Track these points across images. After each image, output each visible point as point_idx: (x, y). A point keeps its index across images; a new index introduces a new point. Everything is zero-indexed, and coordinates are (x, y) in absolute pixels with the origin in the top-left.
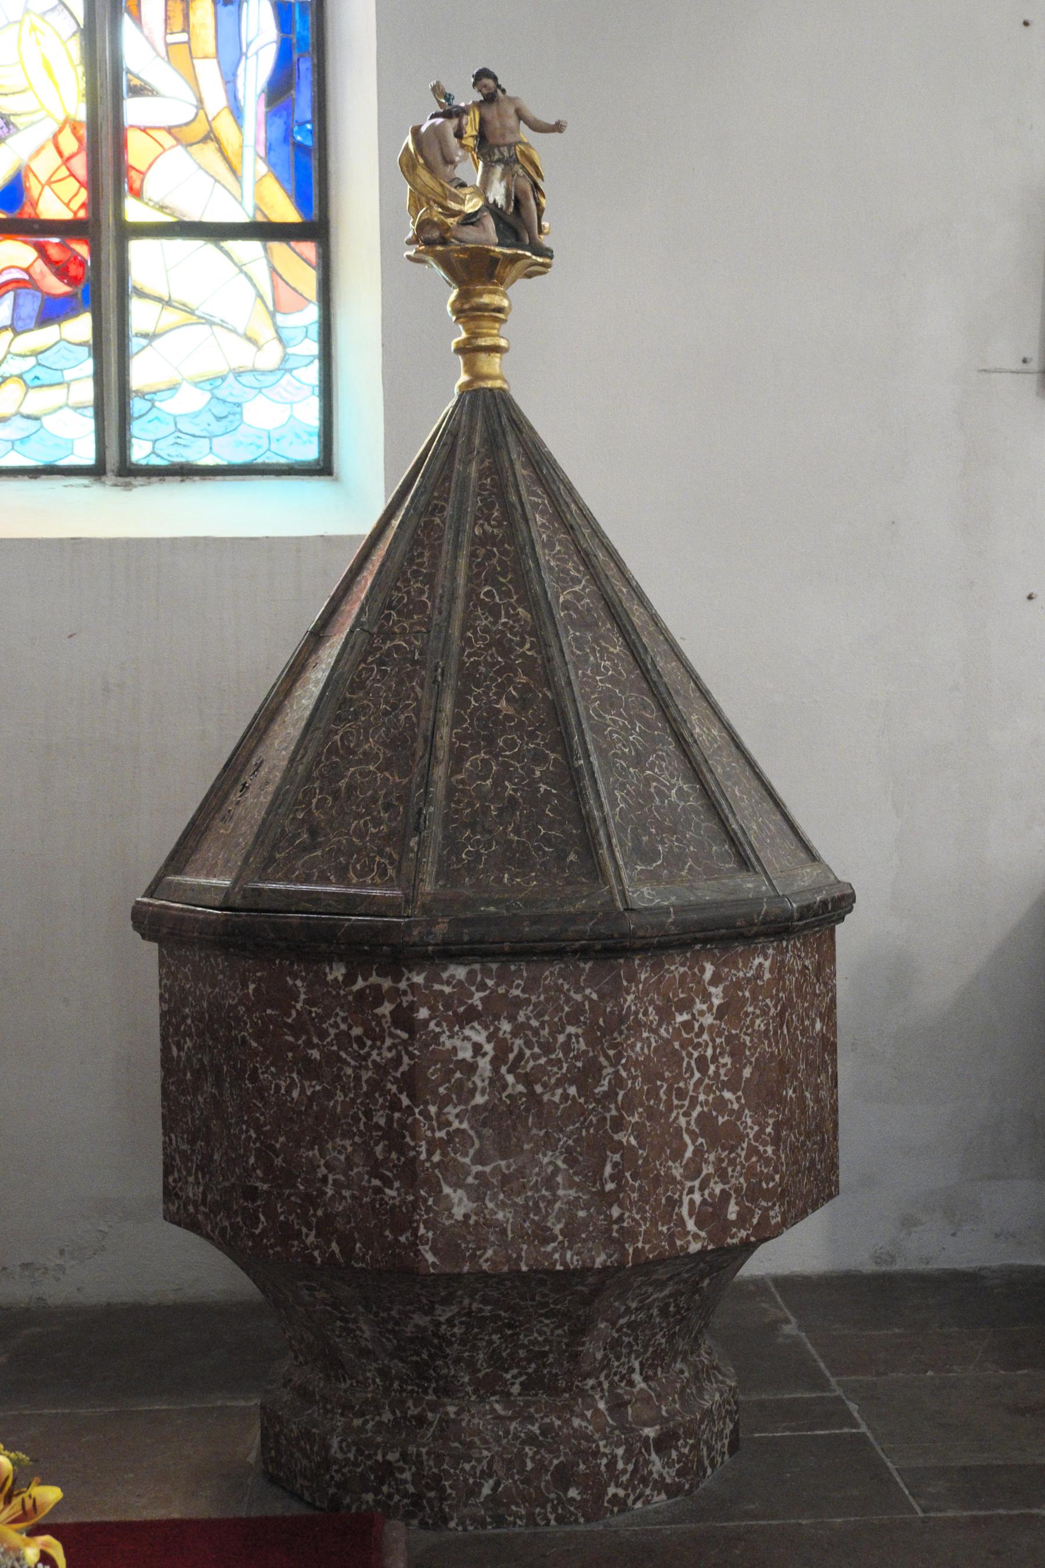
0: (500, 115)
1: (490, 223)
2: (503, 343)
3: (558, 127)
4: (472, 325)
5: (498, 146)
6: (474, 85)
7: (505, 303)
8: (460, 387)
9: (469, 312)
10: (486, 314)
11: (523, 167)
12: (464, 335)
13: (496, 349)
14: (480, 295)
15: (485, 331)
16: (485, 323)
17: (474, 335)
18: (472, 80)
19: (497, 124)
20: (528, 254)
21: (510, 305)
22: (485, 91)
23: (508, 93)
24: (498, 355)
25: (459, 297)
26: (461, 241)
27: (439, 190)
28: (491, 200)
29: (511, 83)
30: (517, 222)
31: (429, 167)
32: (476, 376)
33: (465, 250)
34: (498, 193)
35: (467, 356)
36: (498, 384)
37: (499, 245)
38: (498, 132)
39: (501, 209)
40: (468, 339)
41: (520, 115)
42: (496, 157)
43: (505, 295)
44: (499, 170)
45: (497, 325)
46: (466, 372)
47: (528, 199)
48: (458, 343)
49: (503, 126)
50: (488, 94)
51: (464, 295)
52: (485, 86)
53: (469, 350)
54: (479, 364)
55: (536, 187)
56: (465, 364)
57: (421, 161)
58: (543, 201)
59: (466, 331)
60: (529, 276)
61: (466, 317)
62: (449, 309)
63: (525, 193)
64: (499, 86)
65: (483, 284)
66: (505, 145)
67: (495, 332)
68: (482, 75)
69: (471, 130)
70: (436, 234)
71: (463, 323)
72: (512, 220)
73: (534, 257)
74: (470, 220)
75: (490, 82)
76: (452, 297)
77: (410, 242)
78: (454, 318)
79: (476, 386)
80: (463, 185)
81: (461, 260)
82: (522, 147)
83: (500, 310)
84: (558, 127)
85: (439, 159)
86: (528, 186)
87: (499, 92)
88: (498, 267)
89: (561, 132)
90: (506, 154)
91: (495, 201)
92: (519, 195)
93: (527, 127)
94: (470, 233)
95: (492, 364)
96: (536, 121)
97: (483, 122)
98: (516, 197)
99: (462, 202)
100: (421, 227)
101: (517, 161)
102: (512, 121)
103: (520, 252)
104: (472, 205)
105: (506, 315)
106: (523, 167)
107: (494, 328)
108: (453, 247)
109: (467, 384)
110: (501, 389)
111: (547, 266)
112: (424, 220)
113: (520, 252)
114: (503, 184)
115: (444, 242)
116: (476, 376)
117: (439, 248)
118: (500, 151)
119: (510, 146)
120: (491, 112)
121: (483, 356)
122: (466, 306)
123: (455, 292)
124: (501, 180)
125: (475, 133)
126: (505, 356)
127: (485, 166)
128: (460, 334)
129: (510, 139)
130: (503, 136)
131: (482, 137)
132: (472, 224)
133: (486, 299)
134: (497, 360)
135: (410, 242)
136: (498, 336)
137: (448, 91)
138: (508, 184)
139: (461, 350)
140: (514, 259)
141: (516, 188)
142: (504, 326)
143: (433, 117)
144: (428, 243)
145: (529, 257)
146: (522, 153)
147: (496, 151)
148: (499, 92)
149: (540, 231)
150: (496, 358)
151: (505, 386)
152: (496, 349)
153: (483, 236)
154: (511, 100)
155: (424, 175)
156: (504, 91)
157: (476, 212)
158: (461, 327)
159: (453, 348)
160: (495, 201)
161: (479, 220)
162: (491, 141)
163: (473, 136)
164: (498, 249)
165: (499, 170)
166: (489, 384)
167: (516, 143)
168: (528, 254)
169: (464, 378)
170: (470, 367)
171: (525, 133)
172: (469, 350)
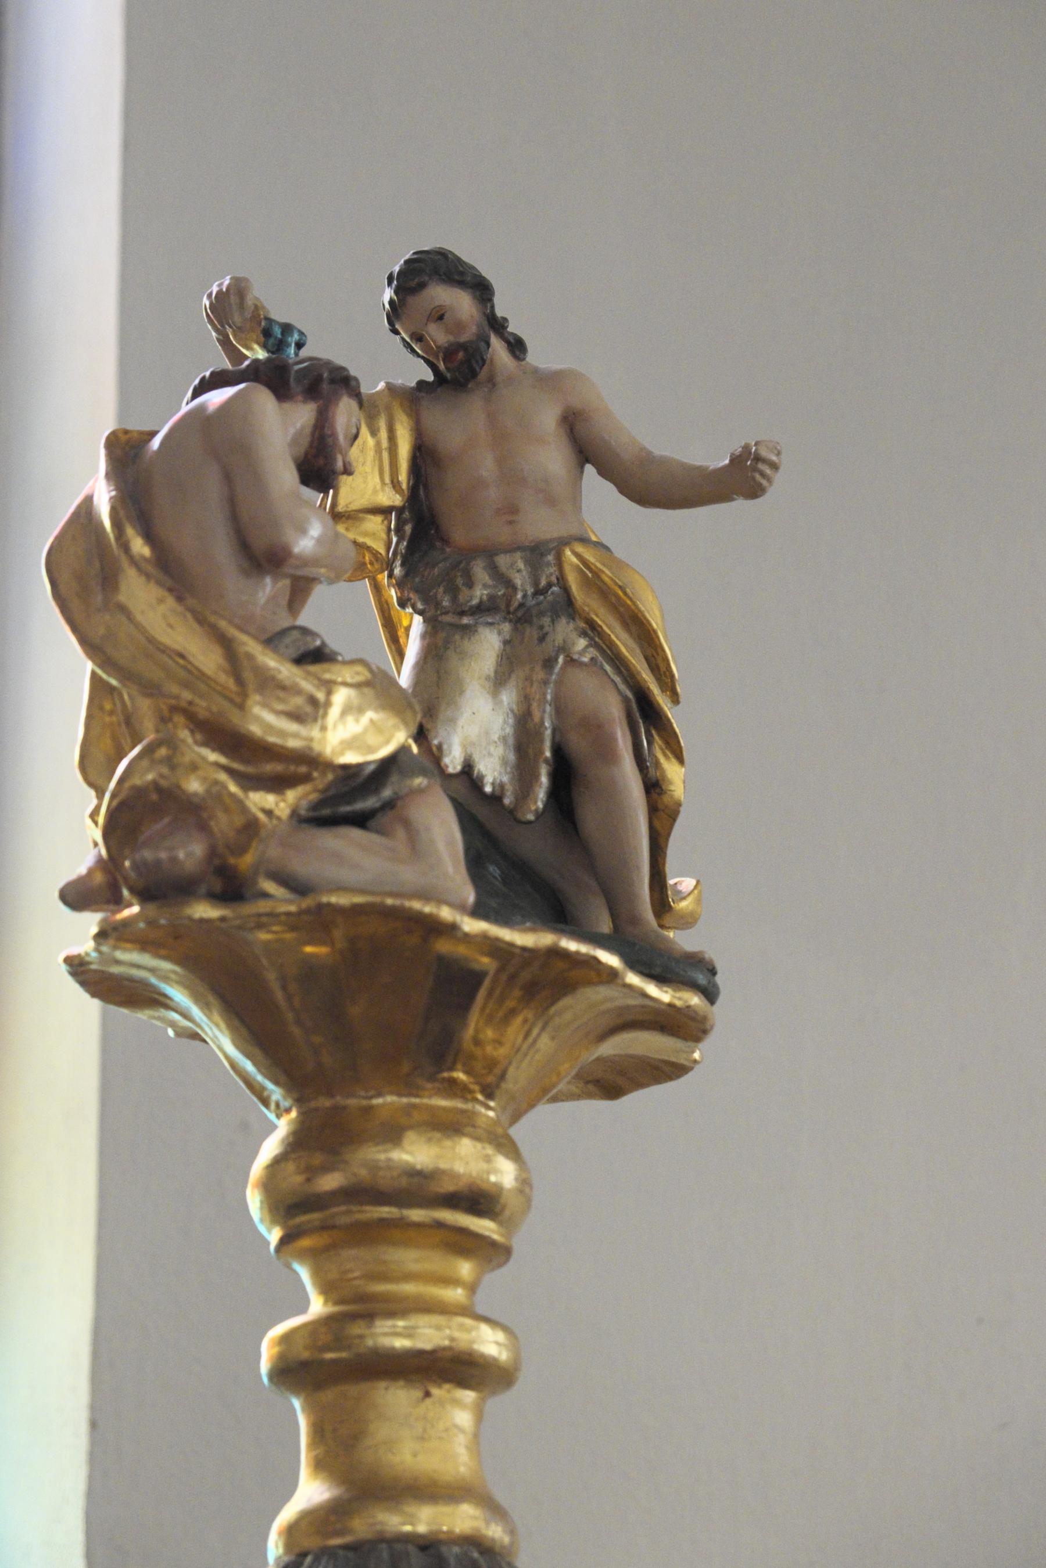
0: (500, 439)
1: (441, 828)
2: (490, 1343)
3: (744, 476)
4: (354, 1260)
5: (490, 553)
6: (395, 313)
7: (504, 1173)
8: (291, 1531)
9: (334, 1209)
10: (417, 1215)
11: (592, 631)
12: (317, 1306)
13: (456, 1368)
14: (393, 1135)
15: (409, 1288)
16: (409, 1258)
17: (357, 1306)
18: (388, 294)
19: (486, 466)
20: (610, 959)
21: (524, 1183)
22: (438, 336)
23: (535, 357)
24: (469, 1396)
25: (298, 1143)
26: (299, 887)
27: (208, 659)
28: (453, 762)
29: (557, 320)
30: (561, 841)
31: (171, 571)
32: (364, 1484)
33: (319, 921)
34: (480, 730)
35: (328, 1395)
36: (463, 1519)
37: (478, 912)
38: (493, 494)
39: (495, 799)
40: (327, 1321)
41: (586, 446)
42: (479, 594)
43: (510, 1148)
44: (488, 644)
45: (465, 1268)
46: (320, 1466)
47: (607, 753)
48: (286, 1339)
49: (512, 476)
50: (449, 353)
51: (316, 1141)
52: (440, 316)
53: (333, 1371)
54: (380, 1431)
55: (646, 713)
56: (318, 1432)
57: (140, 547)
58: (674, 773)
59: (327, 1289)
60: (610, 1083)
61: (325, 1227)
62: (254, 1201)
63: (595, 729)
64: (497, 325)
65: (409, 1087)
66: (512, 549)
67: (456, 1294)
68: (427, 271)
69: (371, 480)
70: (189, 853)
71: (315, 1257)
72: (538, 848)
73: (633, 979)
74: (355, 799)
75: (461, 303)
76: (270, 1148)
77: (76, 897)
78: (274, 1236)
79: (361, 1527)
80: (315, 656)
81: (309, 971)
82: (589, 556)
83: (479, 1200)
84: (744, 476)
85: (222, 551)
86: (611, 706)
87: (498, 347)
88: (474, 1017)
89: (754, 492)
90: (521, 579)
91: (468, 768)
92: (578, 745)
93: (609, 488)
94: (353, 866)
95: (440, 1435)
96: (647, 459)
97: (424, 458)
98: (558, 751)
99: (312, 711)
100: (123, 824)
101: (567, 606)
102: (552, 458)
103: (572, 945)
104: (352, 732)
105: (509, 1225)
106: (592, 631)
107: (450, 1281)
108: (262, 906)
109: (318, 1520)
110: (474, 1542)
111: (686, 1027)
112: (139, 793)
113: (572, 945)
114: (508, 697)
115: (232, 888)
116: (364, 1484)
117: (204, 911)
118: (494, 570)
119: (536, 553)
120: (459, 426)
121: (396, 1398)
122: (330, 1182)
123: (280, 1130)
124: (499, 681)
125: (391, 498)
126: (500, 1403)
127: (433, 625)
128: (303, 1306)
129: (540, 524)
130: (511, 511)
131: (422, 523)
132: (361, 821)
133: (416, 1153)
134: (463, 1418)
135: (76, 897)
136: (466, 1311)
137: (279, 314)
138: (526, 699)
139: (295, 1372)
140: (548, 980)
141: (560, 710)
142: (498, 1279)
143: (198, 392)
144: (161, 889)
145: (612, 976)
146: (594, 581)
147: (480, 572)
148: (498, 347)
149: (662, 902)
150: (459, 1409)
151: (495, 1532)
152: (456, 1368)
153: (408, 875)
154: (550, 381)
155: (145, 600)
156: (517, 347)
157: (388, 766)
158: (304, 1273)
159: (265, 1366)
160: (468, 768)
161: (389, 805)
162: (459, 534)
163: (384, 511)
164: (471, 926)
165: (488, 644)
166: (422, 1520)
167: (565, 542)
168: (610, 959)
169: (311, 1491)
170: (339, 1445)
171: (602, 508)
172: (333, 1371)
